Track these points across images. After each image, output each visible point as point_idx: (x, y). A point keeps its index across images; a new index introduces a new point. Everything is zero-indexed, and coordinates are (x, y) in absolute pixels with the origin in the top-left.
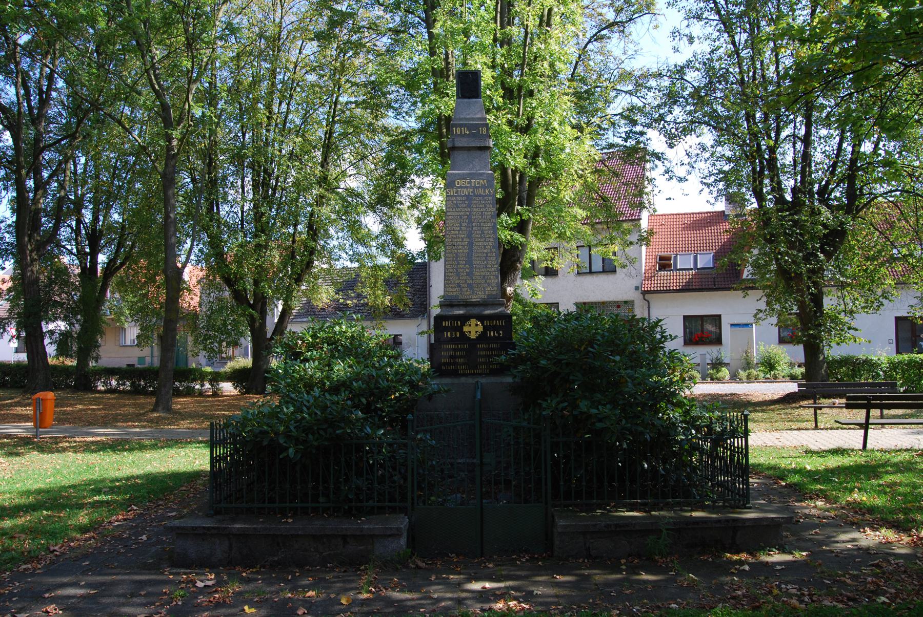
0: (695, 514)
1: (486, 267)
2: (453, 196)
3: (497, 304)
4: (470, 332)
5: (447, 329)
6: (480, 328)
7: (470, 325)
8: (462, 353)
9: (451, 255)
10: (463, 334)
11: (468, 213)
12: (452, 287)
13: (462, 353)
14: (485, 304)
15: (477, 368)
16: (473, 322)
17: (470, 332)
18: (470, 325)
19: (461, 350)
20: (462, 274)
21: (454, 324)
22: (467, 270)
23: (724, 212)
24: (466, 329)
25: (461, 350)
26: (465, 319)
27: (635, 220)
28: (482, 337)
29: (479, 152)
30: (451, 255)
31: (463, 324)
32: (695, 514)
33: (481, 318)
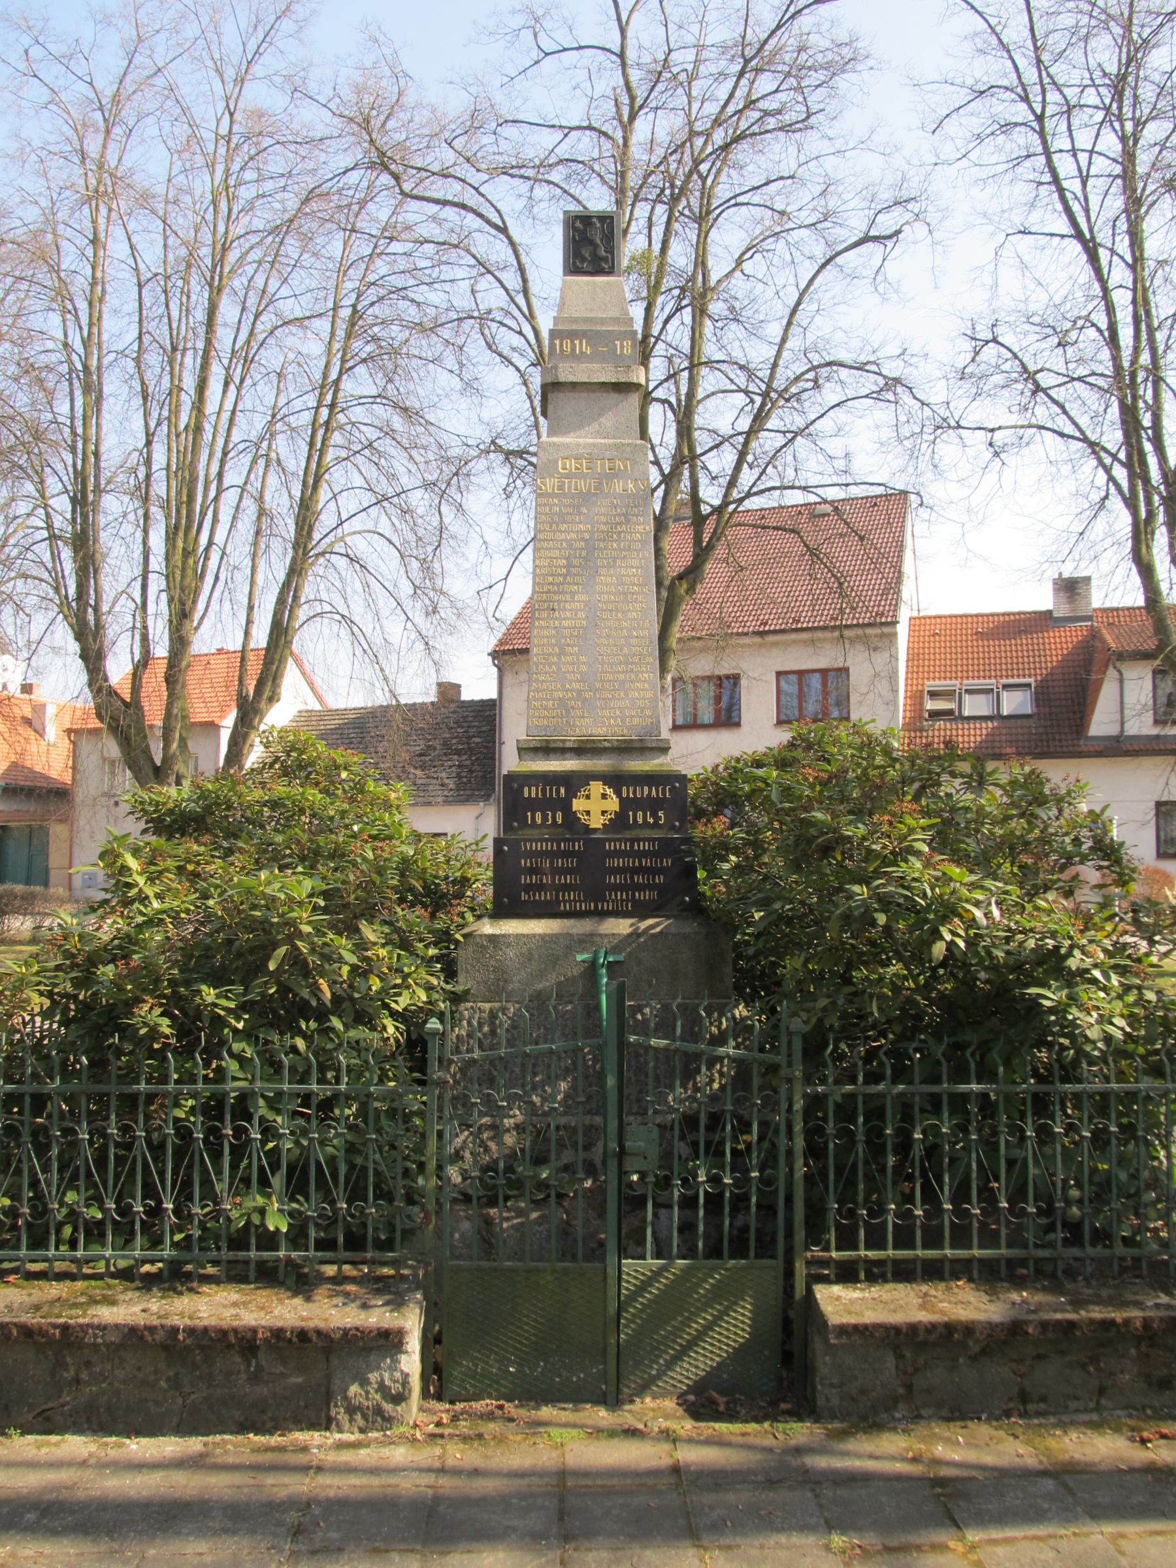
0: (604, 998)
1: (627, 663)
2: (553, 495)
3: (652, 749)
4: (588, 813)
5: (533, 805)
6: (613, 804)
7: (588, 797)
8: (573, 863)
9: (546, 633)
10: (571, 819)
11: (587, 536)
12: (546, 708)
13: (573, 863)
14: (626, 748)
15: (604, 900)
16: (597, 788)
17: (588, 813)
18: (588, 797)
19: (567, 854)
20: (570, 677)
21: (552, 792)
22: (584, 668)
23: (1050, 612)
24: (578, 805)
25: (567, 854)
26: (574, 783)
27: (886, 624)
28: (619, 822)
29: (614, 397)
30: (546, 633)
31: (572, 793)
32: (604, 998)
33: (615, 780)
